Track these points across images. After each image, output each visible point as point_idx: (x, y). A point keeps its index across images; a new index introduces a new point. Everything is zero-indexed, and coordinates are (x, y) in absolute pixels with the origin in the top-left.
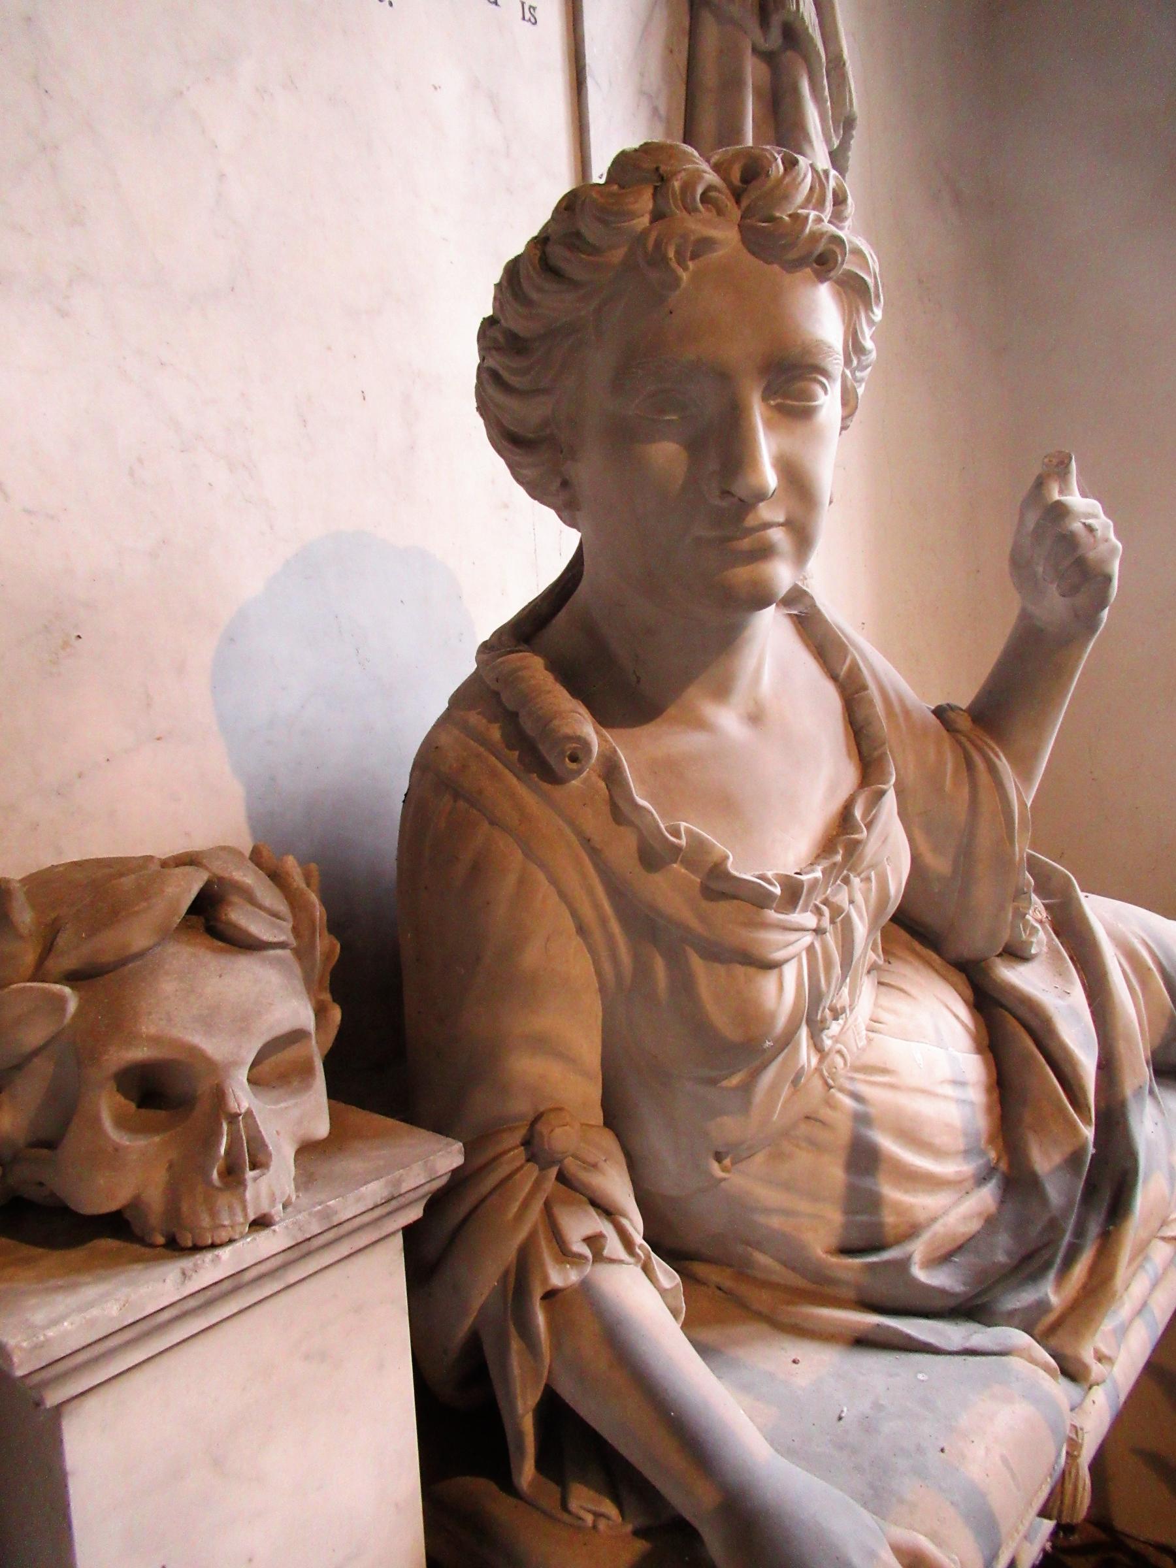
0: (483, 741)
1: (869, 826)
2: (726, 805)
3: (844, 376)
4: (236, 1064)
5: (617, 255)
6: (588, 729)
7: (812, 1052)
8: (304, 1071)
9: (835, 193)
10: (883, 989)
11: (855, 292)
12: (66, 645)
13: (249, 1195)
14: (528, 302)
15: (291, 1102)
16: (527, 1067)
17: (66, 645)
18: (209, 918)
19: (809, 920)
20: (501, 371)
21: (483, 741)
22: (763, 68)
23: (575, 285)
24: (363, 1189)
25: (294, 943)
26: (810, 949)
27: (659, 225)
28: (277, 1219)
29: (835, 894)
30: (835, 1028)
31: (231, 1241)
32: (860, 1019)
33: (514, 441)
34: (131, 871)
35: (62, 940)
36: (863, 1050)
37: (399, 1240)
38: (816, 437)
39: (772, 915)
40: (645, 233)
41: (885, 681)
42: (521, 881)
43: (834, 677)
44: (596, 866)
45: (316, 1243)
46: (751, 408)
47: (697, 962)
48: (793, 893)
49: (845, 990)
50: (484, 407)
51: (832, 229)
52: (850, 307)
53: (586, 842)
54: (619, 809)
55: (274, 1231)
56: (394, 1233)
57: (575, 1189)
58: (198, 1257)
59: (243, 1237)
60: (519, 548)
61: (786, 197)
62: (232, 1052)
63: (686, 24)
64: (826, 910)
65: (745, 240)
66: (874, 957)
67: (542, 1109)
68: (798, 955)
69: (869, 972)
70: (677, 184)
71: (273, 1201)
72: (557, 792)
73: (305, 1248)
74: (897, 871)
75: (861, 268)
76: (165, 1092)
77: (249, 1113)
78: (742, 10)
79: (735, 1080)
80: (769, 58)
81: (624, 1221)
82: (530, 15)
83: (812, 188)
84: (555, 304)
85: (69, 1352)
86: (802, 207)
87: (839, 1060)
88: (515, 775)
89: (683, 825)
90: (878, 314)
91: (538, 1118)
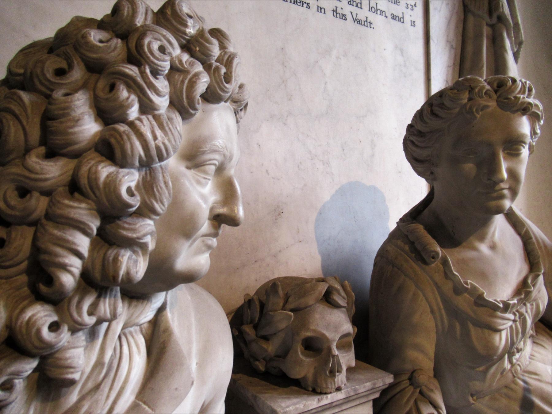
0: (403, 250)
1: (534, 286)
2: (484, 276)
4: (334, 340)
5: (457, 110)
6: (439, 249)
8: (350, 346)
9: (528, 88)
10: (535, 344)
11: (534, 118)
12: (279, 214)
13: (336, 380)
14: (425, 123)
16: (412, 354)
17: (279, 214)
18: (327, 298)
19: (511, 317)
20: (415, 141)
21: (403, 250)
22: (489, 29)
23: (441, 118)
24: (365, 384)
26: (511, 327)
27: (470, 103)
29: (521, 309)
30: (517, 356)
31: (330, 393)
32: (526, 354)
34: (308, 283)
35: (290, 300)
36: (527, 365)
37: (371, 403)
38: (520, 162)
39: (499, 314)
40: (465, 105)
41: (538, 235)
42: (414, 294)
43: (519, 234)
44: (439, 292)
45: (351, 398)
46: (499, 154)
47: (471, 326)
48: (507, 307)
49: (522, 343)
53: (436, 284)
54: (447, 274)
57: (426, 398)
58: (322, 396)
59: (334, 392)
60: (409, 189)
61: (513, 92)
62: (333, 336)
63: (462, 17)
64: (517, 314)
65: (498, 105)
67: (415, 368)
68: (507, 328)
69: (529, 337)
70: (477, 90)
71: (342, 381)
72: (427, 268)
74: (543, 302)
76: (315, 346)
77: (337, 356)
78: (483, 12)
79: (481, 369)
80: (492, 26)
81: (441, 411)
82: (413, 24)
83: (521, 88)
84: (434, 123)
87: (518, 368)
88: (413, 261)
89: (469, 281)
90: (542, 122)
91: (414, 371)
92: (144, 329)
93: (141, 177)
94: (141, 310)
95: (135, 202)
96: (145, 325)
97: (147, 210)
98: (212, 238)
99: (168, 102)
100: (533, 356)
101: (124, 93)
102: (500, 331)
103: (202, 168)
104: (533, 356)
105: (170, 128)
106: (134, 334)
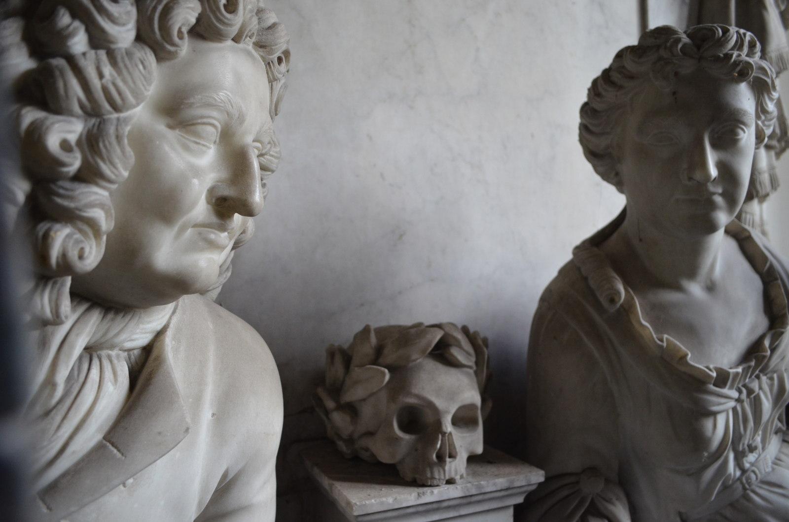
2: (691, 331)
3: (757, 125)
4: (447, 412)
6: (621, 287)
7: (737, 469)
9: (749, 42)
10: (786, 444)
15: (468, 435)
18: (441, 353)
19: (734, 394)
20: (589, 125)
24: (497, 480)
25: (475, 368)
28: (457, 481)
31: (437, 486)
32: (768, 457)
33: (593, 155)
36: (768, 473)
37: (511, 511)
50: (582, 140)
51: (748, 59)
52: (758, 93)
55: (457, 488)
56: (507, 507)
58: (425, 489)
60: (601, 204)
62: (448, 410)
64: (744, 391)
66: (780, 425)
68: (727, 411)
71: (456, 472)
73: (469, 500)
75: (763, 74)
76: (420, 422)
77: (450, 434)
83: (737, 41)
84: (610, 95)
85: (373, 512)
86: (730, 50)
87: (753, 476)
92: (133, 357)
93: (87, 129)
94: (122, 326)
95: (74, 163)
96: (136, 352)
97: (88, 174)
98: (216, 232)
99: (132, 35)
100: (780, 460)
101: (64, 19)
102: (714, 414)
103: (192, 128)
104: (780, 460)
105: (125, 66)
106: (115, 361)
